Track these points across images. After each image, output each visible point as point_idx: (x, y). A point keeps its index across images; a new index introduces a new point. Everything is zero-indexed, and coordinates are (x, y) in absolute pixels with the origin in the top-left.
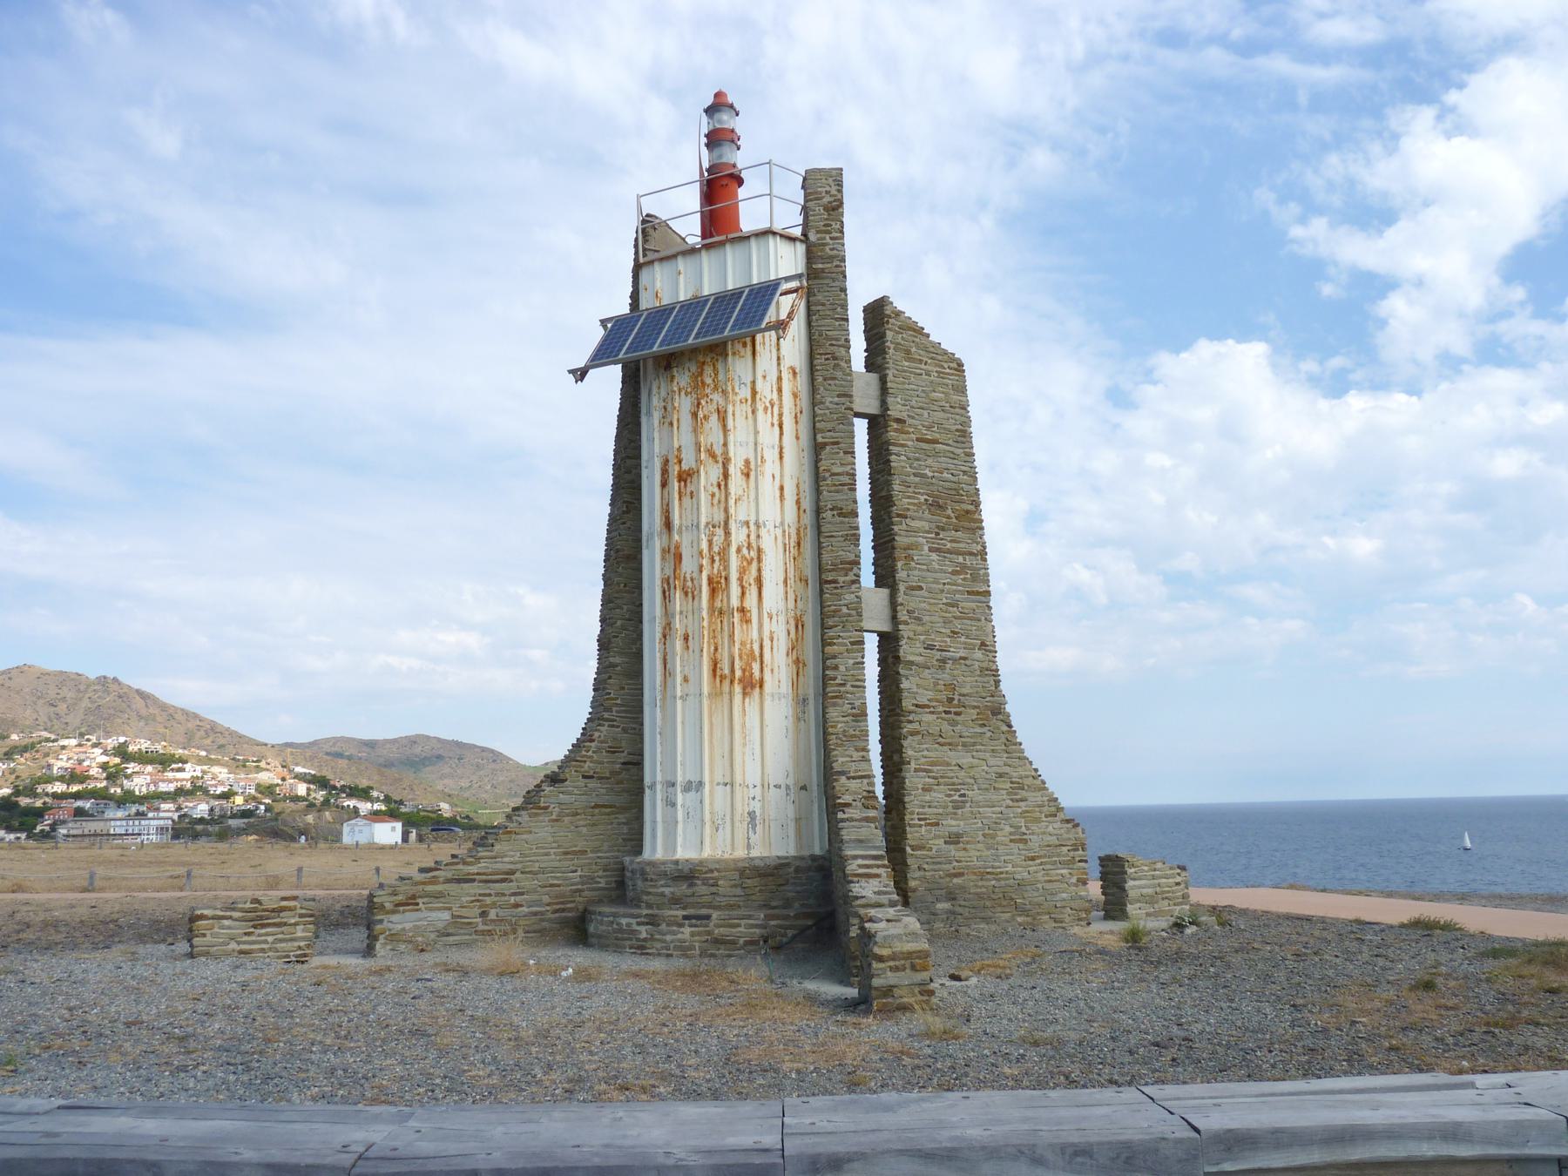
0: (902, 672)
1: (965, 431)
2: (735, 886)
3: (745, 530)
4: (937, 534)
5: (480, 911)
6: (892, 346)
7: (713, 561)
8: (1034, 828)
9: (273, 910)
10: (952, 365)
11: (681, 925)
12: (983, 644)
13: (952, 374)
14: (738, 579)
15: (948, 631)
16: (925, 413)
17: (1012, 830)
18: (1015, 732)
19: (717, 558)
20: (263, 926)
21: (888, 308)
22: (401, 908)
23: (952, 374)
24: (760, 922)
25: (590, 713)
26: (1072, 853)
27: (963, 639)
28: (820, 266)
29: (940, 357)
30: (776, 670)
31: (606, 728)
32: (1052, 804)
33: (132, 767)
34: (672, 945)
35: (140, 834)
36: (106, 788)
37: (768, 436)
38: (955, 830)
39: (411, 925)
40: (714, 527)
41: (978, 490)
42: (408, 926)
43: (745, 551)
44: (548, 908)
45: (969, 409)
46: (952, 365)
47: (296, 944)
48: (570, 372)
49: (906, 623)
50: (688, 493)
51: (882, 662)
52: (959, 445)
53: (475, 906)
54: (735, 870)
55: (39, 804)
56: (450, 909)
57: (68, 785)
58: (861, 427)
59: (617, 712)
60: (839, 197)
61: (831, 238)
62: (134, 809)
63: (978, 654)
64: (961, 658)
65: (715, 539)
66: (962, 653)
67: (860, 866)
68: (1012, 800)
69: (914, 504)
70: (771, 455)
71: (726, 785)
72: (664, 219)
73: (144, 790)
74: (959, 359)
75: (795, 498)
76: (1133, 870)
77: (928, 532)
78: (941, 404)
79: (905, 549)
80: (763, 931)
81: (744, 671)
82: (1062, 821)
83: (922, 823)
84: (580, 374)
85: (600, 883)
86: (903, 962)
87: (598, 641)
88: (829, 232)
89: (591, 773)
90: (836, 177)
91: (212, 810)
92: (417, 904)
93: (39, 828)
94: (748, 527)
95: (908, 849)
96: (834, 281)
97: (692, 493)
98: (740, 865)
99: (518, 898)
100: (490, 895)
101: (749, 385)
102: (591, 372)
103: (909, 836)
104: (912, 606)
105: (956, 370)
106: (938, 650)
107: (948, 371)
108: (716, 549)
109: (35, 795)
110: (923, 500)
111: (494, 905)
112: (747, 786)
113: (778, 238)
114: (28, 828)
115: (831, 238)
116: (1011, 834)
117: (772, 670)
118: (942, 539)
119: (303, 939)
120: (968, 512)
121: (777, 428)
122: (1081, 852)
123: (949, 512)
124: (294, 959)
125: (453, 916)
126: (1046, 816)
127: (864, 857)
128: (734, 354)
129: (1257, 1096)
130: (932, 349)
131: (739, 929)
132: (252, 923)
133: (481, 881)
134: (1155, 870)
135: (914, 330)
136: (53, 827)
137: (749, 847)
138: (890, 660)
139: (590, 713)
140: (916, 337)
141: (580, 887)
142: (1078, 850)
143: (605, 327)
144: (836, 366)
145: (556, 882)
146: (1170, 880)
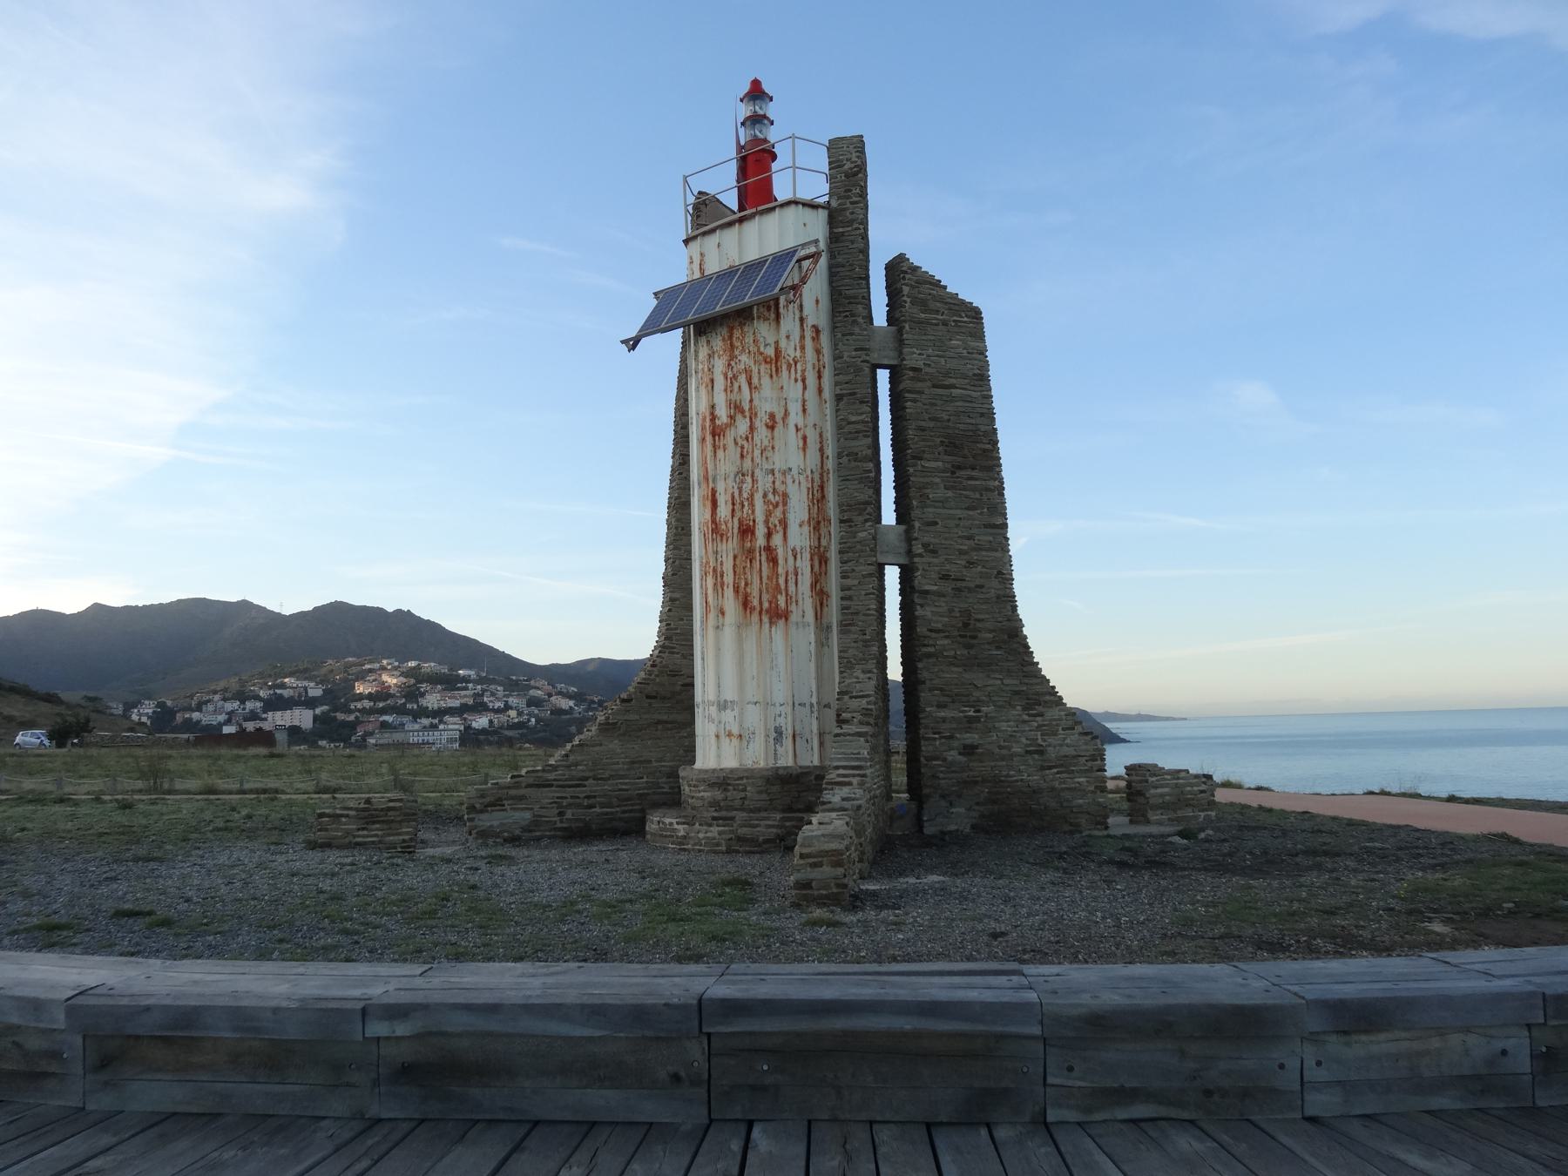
0: (916, 600)
1: (982, 375)
2: (760, 792)
3: (770, 478)
4: (953, 473)
5: (557, 811)
6: (908, 300)
7: (743, 506)
8: (1051, 740)
9: (382, 810)
10: (969, 313)
11: (710, 825)
12: (1000, 573)
13: (971, 322)
14: (765, 521)
15: (964, 563)
16: (942, 360)
17: (1028, 742)
18: (1032, 652)
19: (746, 504)
20: (374, 823)
21: (904, 264)
22: (489, 809)
23: (971, 322)
24: (777, 823)
25: (657, 642)
26: (1089, 764)
27: (979, 568)
28: (841, 230)
29: (957, 308)
30: (800, 602)
31: (667, 654)
32: (1069, 718)
33: (424, 687)
34: (703, 842)
35: (434, 744)
36: (405, 704)
37: (794, 392)
38: (968, 742)
39: (498, 823)
40: (743, 475)
41: (996, 430)
42: (495, 823)
43: (771, 496)
44: (618, 809)
45: (987, 354)
46: (969, 313)
47: (401, 838)
48: (623, 342)
49: (920, 555)
50: (721, 446)
51: (902, 592)
52: (975, 389)
53: (553, 807)
54: (760, 778)
55: (352, 718)
56: (532, 809)
57: (375, 702)
58: (883, 376)
59: (677, 640)
60: (859, 163)
61: (852, 203)
62: (426, 721)
63: (995, 583)
64: (977, 586)
65: (744, 486)
66: (978, 582)
67: (839, 775)
68: (1029, 715)
69: (929, 446)
70: (794, 408)
71: (756, 703)
72: (713, 193)
73: (436, 707)
74: (977, 307)
75: (818, 446)
76: (1154, 779)
77: (944, 471)
78: (958, 351)
79: (920, 488)
80: (779, 831)
81: (770, 603)
82: (1080, 734)
83: (937, 736)
84: (632, 344)
85: (664, 788)
86: (820, 859)
87: (663, 578)
88: (849, 197)
89: (654, 694)
90: (858, 144)
91: (491, 722)
92: (504, 805)
93: (353, 738)
94: (774, 475)
95: (922, 759)
96: (853, 244)
97: (724, 445)
98: (765, 773)
99: (592, 801)
100: (566, 798)
101: (773, 345)
102: (643, 340)
103: (923, 748)
104: (926, 539)
105: (973, 318)
106: (954, 580)
107: (966, 319)
108: (745, 495)
109: (350, 712)
110: (938, 442)
111: (569, 806)
112: (774, 705)
113: (801, 206)
114: (346, 740)
115: (852, 203)
116: (1027, 745)
117: (797, 601)
118: (958, 477)
119: (407, 833)
120: (985, 451)
121: (800, 384)
122: (1099, 762)
123: (966, 451)
124: (400, 850)
125: (534, 816)
126: (1063, 729)
127: (845, 767)
128: (759, 318)
129: (813, 974)
130: (949, 300)
131: (758, 829)
132: (366, 820)
133: (558, 786)
134: (1178, 778)
135: (931, 283)
136: (364, 738)
137: (776, 758)
138: (908, 590)
139: (657, 642)
140: (933, 290)
141: (646, 791)
142: (1096, 760)
143: (657, 298)
144: (855, 322)
145: (624, 787)
146: (1195, 788)
